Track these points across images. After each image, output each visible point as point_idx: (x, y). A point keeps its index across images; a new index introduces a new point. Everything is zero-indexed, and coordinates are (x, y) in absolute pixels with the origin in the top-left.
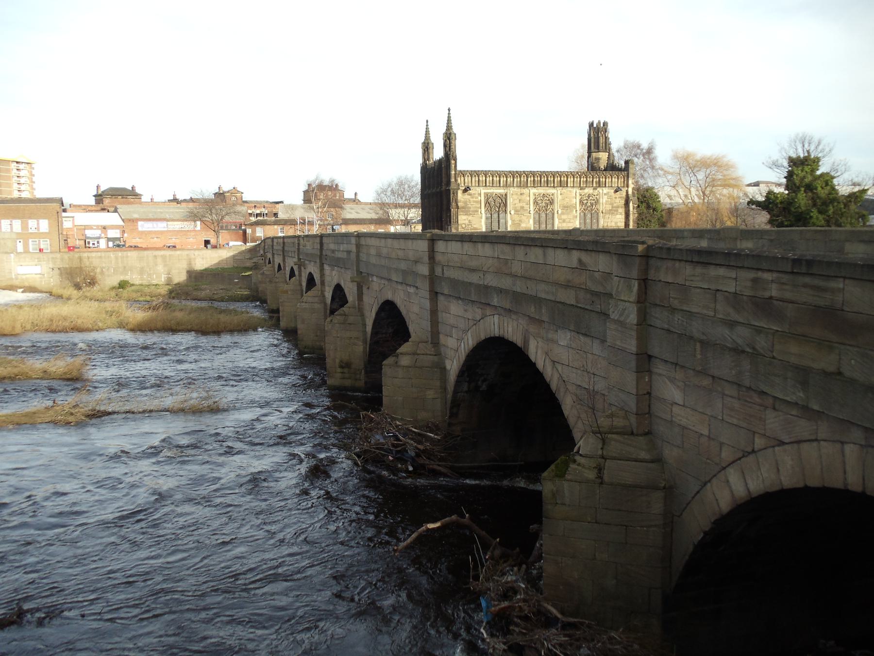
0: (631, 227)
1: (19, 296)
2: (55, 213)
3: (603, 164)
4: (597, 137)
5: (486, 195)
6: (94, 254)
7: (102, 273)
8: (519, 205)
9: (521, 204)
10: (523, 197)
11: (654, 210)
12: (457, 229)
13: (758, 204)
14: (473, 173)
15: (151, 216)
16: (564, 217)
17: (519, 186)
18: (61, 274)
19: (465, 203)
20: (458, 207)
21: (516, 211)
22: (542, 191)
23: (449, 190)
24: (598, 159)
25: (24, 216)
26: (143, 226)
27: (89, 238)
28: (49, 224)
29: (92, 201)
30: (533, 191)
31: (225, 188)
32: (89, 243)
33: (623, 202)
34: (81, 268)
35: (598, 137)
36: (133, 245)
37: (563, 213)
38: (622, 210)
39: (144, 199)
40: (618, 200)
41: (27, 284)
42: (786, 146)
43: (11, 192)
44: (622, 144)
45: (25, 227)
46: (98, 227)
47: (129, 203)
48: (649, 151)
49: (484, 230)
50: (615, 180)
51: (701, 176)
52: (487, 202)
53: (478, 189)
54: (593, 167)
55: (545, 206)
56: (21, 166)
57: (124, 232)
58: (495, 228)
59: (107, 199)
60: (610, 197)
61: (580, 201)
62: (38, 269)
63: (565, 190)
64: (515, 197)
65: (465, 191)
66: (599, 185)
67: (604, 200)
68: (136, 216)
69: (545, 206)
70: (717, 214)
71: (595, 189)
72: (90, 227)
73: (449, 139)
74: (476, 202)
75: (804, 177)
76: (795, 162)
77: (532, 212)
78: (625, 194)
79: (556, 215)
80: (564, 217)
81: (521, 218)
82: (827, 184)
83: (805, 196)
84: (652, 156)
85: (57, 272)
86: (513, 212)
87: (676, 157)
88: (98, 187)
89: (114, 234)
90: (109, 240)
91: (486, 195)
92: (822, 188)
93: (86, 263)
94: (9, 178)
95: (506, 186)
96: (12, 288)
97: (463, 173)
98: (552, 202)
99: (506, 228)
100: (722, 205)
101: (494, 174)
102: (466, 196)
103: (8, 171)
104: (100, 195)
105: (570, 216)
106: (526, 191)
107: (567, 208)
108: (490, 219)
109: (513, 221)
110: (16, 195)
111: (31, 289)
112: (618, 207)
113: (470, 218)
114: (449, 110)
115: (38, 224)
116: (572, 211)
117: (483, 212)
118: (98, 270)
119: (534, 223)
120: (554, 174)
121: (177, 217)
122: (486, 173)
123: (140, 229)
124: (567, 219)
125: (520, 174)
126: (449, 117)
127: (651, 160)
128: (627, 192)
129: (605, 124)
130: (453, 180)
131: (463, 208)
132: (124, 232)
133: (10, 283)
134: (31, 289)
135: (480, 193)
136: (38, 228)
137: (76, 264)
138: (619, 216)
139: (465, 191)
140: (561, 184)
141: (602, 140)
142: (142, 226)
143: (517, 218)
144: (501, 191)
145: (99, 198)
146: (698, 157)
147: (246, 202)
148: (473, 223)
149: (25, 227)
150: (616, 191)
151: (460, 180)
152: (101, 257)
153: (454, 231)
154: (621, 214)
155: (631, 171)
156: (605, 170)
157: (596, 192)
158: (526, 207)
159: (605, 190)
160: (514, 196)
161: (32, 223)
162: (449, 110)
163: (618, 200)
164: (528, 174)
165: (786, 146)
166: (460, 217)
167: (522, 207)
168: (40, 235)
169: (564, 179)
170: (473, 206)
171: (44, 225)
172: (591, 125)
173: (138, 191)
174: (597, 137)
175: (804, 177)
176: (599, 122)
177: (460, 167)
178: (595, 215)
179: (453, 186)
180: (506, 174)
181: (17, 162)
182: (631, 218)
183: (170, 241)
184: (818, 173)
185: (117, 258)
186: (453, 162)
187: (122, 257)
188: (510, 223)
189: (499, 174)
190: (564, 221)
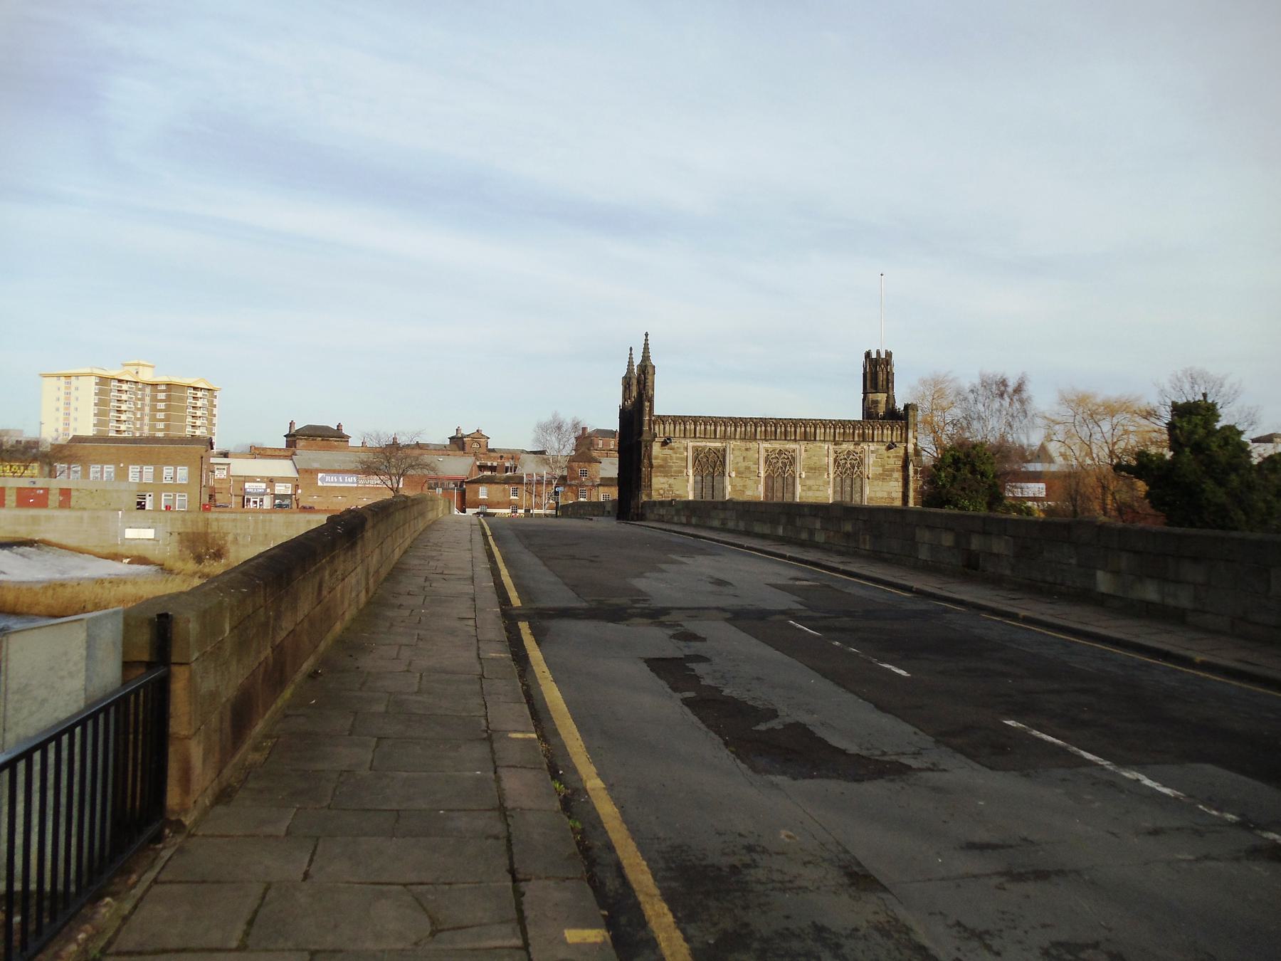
0: (911, 504)
1: (122, 568)
2: (198, 459)
3: (881, 410)
4: (877, 372)
5: (696, 449)
6: (226, 516)
7: (236, 540)
8: (742, 465)
9: (746, 464)
10: (749, 453)
11: (983, 474)
12: (650, 495)
13: (1128, 468)
14: (676, 420)
15: (337, 467)
16: (809, 482)
17: (743, 439)
18: (181, 542)
19: (665, 460)
20: (651, 466)
21: (739, 473)
22: (777, 445)
23: (640, 443)
24: (876, 402)
25: (158, 462)
26: (324, 480)
27: (249, 493)
28: (190, 473)
29: (282, 444)
30: (767, 445)
31: (465, 432)
32: (249, 500)
33: (900, 463)
34: (206, 534)
35: (876, 373)
36: (308, 505)
37: (807, 477)
38: (898, 475)
39: (352, 443)
40: (892, 461)
41: (135, 553)
42: (1168, 387)
43: (183, 428)
44: (977, 381)
45: (158, 475)
46: (262, 479)
47: (331, 448)
48: (1018, 390)
49: (691, 498)
50: (887, 432)
51: (1106, 426)
52: (696, 459)
53: (684, 442)
54: (869, 413)
55: (781, 469)
56: (200, 394)
57: (297, 487)
58: (848, 499)
59: (458, 442)
60: (880, 457)
61: (835, 461)
62: (150, 533)
63: (811, 445)
64: (737, 453)
65: (664, 444)
66: (864, 438)
67: (871, 460)
68: (316, 465)
69: (781, 469)
70: (1078, 484)
71: (857, 444)
72: (252, 479)
73: (644, 372)
74: (681, 459)
75: (1192, 433)
76: (1180, 411)
77: (762, 474)
78: (902, 452)
79: (798, 480)
80: (809, 482)
81: (746, 480)
82: (1227, 443)
83: (1194, 462)
84: (1025, 395)
85: (176, 537)
86: (733, 475)
87: (1065, 400)
88: (291, 424)
89: (281, 489)
90: (276, 497)
91: (696, 449)
92: (1220, 447)
93: (214, 527)
94: (184, 409)
95: (725, 437)
96: (116, 557)
97: (663, 419)
98: (792, 461)
99: (724, 496)
100: (1104, 469)
101: (707, 420)
102: (667, 451)
103: (183, 399)
104: (294, 435)
105: (820, 482)
106: (754, 445)
107: (814, 470)
108: (700, 485)
109: (733, 486)
110: (188, 431)
111: (141, 560)
112: (893, 470)
113: (671, 481)
114: (647, 335)
115: (175, 472)
116: (821, 475)
117: (691, 472)
118: (230, 538)
119: (766, 490)
120: (795, 423)
121: (352, 466)
122: (695, 420)
123: (320, 484)
124: (816, 485)
125: (744, 421)
126: (646, 345)
127: (1022, 402)
128: (906, 448)
129: (889, 354)
130: (646, 428)
131: (661, 466)
132: (297, 487)
133: (113, 550)
134: (141, 560)
135: (687, 447)
136: (173, 478)
137: (201, 528)
138: (892, 484)
139: (664, 444)
140: (806, 437)
141: (881, 376)
142: (323, 480)
143: (739, 483)
144: (718, 445)
145: (293, 438)
146: (1099, 400)
147: (493, 450)
148: (675, 488)
149: (158, 475)
150: (889, 448)
151: (658, 429)
152: (234, 520)
153: (645, 498)
154: (897, 480)
155: (911, 419)
156: (883, 418)
157: (859, 449)
158: (754, 467)
159: (873, 447)
160: (735, 452)
161: (167, 471)
162: (647, 335)
163: (892, 461)
164: (756, 422)
165: (1168, 387)
166: (654, 480)
167: (748, 468)
168: (175, 487)
169: (810, 430)
170: (675, 464)
171: (183, 473)
172: (868, 355)
173: (345, 432)
174: (877, 372)
175: (1192, 433)
176: (878, 353)
177: (657, 412)
178: (789, 483)
179: (645, 437)
180: (725, 421)
181: (195, 388)
182: (912, 486)
183: (310, 499)
184: (1218, 426)
185: (256, 522)
186: (647, 404)
187: (264, 521)
188: (729, 488)
189: (715, 421)
190: (810, 488)
